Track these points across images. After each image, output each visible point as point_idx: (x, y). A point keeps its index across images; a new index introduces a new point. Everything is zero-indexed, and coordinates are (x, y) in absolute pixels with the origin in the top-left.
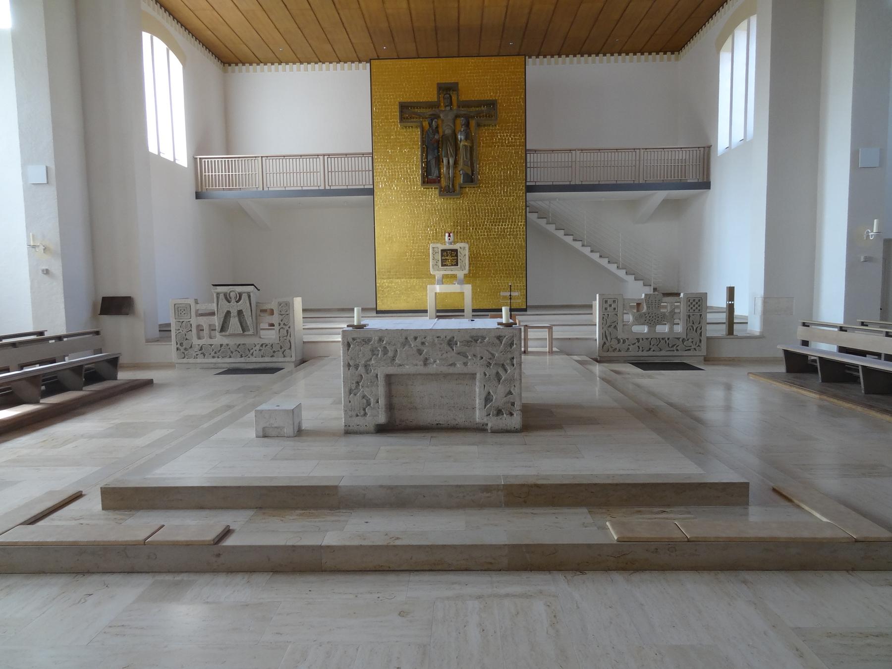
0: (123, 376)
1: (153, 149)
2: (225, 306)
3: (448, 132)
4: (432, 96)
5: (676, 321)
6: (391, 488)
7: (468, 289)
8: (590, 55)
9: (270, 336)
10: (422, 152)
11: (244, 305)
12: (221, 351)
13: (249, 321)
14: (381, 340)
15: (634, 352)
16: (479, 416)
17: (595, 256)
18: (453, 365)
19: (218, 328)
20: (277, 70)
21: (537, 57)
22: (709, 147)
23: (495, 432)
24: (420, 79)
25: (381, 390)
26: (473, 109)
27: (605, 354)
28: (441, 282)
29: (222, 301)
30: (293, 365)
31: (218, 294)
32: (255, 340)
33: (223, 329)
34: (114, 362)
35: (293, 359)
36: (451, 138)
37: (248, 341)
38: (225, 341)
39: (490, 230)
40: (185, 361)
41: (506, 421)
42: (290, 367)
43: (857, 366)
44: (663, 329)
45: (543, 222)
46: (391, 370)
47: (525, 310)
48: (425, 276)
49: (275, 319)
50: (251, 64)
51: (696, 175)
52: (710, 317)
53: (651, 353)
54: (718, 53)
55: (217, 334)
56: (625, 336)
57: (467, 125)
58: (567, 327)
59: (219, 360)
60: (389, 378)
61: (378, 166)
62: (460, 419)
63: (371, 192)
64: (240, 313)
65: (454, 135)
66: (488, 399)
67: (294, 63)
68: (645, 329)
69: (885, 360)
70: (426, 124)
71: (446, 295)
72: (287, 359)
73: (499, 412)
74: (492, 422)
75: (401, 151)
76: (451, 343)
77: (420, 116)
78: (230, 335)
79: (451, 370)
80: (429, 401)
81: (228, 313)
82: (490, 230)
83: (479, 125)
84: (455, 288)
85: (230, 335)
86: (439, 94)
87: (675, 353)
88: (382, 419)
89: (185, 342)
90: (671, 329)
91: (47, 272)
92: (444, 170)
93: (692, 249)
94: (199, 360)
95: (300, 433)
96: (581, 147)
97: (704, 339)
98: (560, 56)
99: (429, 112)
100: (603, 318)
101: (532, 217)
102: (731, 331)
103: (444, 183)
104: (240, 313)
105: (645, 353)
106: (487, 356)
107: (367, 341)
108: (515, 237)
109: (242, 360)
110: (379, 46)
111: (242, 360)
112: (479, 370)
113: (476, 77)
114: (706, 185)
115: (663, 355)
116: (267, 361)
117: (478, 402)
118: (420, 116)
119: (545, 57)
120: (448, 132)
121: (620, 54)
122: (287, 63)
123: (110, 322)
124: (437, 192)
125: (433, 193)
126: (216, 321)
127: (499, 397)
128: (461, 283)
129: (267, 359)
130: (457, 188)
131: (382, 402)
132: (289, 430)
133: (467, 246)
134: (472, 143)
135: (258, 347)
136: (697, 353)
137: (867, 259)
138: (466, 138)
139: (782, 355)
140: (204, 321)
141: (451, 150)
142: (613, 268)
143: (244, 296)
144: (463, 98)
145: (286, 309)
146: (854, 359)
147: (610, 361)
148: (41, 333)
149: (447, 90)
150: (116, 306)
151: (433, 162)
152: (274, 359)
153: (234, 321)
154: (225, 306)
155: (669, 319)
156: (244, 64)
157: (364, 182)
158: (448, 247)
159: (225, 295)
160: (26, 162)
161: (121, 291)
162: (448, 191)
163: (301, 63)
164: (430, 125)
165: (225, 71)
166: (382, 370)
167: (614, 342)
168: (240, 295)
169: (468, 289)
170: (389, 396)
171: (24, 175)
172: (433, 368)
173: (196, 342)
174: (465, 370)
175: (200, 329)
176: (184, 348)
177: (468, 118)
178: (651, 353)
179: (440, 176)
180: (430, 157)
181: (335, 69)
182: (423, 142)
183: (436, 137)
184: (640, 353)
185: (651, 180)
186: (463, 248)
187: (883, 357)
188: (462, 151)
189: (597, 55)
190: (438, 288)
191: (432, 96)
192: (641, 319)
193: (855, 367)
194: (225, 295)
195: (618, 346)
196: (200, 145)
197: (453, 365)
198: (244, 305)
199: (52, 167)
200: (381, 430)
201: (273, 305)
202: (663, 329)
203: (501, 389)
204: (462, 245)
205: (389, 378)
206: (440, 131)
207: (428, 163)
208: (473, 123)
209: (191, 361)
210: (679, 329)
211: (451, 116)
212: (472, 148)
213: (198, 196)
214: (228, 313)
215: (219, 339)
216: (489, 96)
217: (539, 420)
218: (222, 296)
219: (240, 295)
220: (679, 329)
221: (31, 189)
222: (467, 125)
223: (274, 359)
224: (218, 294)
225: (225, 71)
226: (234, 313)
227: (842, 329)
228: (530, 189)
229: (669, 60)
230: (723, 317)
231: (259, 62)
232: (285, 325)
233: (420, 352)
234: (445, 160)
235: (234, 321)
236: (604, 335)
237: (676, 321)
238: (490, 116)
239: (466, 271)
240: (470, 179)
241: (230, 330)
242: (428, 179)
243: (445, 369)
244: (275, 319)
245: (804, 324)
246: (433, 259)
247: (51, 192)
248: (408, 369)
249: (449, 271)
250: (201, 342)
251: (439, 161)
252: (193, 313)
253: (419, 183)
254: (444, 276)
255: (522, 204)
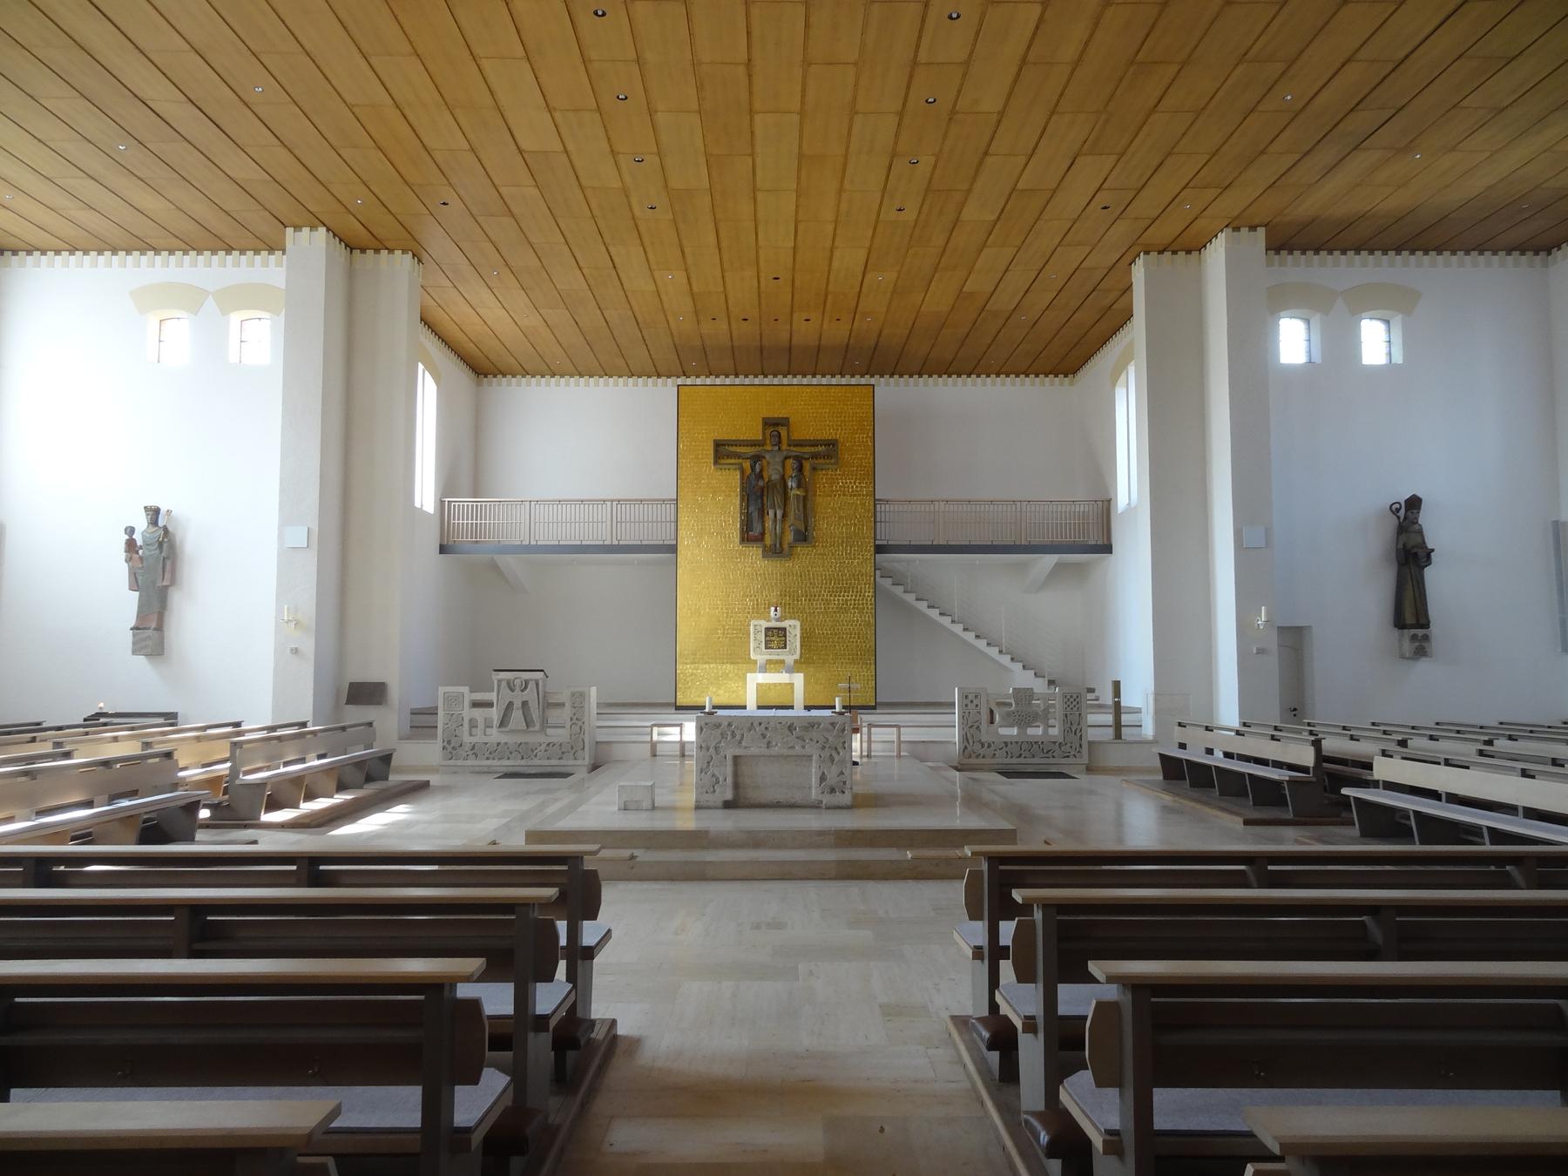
0: (394, 778)
1: (417, 504)
2: (507, 695)
3: (775, 477)
4: (756, 433)
5: (1051, 722)
6: (749, 832)
7: (798, 679)
8: (959, 375)
9: (560, 735)
10: (742, 500)
11: (530, 695)
12: (496, 751)
13: (535, 714)
14: (730, 725)
15: (1002, 759)
16: (814, 794)
17: (970, 637)
18: (792, 747)
19: (496, 722)
20: (548, 384)
21: (892, 375)
22: (1109, 501)
23: (828, 808)
24: (744, 403)
25: (729, 769)
26: (807, 449)
27: (967, 761)
28: (764, 669)
29: (505, 690)
30: (585, 770)
31: (499, 681)
32: (541, 739)
33: (503, 723)
34: (386, 759)
35: (587, 762)
36: (780, 487)
37: (532, 739)
38: (503, 739)
39: (828, 602)
40: (452, 762)
41: (840, 799)
42: (582, 773)
43: (1479, 827)
44: (1030, 731)
45: (899, 590)
46: (738, 752)
47: (874, 708)
48: (738, 657)
49: (566, 713)
50: (514, 376)
51: (1093, 538)
52: (1093, 718)
53: (1022, 760)
54: (1114, 385)
55: (494, 731)
56: (990, 740)
57: (800, 469)
58: (917, 728)
59: (495, 762)
60: (736, 759)
61: (684, 519)
62: (798, 797)
63: (673, 549)
64: (525, 704)
65: (783, 479)
66: (823, 778)
67: (572, 376)
68: (1015, 731)
69: (1526, 816)
70: (747, 465)
71: (769, 686)
72: (579, 762)
73: (833, 790)
74: (827, 799)
75: (713, 498)
76: (791, 728)
77: (738, 456)
78: (512, 731)
79: (791, 752)
80: (768, 779)
81: (511, 704)
82: (828, 602)
83: (814, 469)
84: (782, 678)
85: (512, 731)
86: (764, 430)
87: (1051, 761)
88: (729, 796)
89: (453, 740)
90: (1046, 732)
91: (295, 651)
92: (769, 524)
93: (1097, 628)
94: (469, 763)
95: (654, 808)
96: (945, 497)
97: (1085, 746)
98: (920, 376)
99: (750, 451)
100: (962, 717)
101: (886, 583)
102: (1118, 735)
103: (768, 540)
104: (525, 704)
105: (1015, 760)
106: (822, 740)
107: (718, 726)
108: (861, 611)
109: (523, 762)
110: (685, 360)
111: (523, 762)
112: (812, 750)
113: (807, 401)
114: (1108, 549)
115: (1038, 762)
116: (554, 764)
117: (814, 780)
118: (738, 456)
119: (901, 376)
120: (775, 477)
121: (998, 375)
122: (562, 376)
123: (357, 714)
124: (760, 551)
125: (755, 552)
126: (494, 714)
127: (832, 778)
128: (790, 670)
129: (554, 762)
130: (786, 546)
131: (730, 780)
132: (646, 804)
133: (798, 624)
134: (807, 491)
135: (543, 747)
136: (1078, 761)
137: (1261, 651)
138: (799, 486)
139: (1157, 763)
140: (478, 713)
141: (778, 500)
142: (993, 652)
143: (532, 685)
144: (796, 436)
145: (579, 699)
146: (1476, 816)
147: (973, 769)
148: (238, 725)
149: (774, 425)
150: (366, 693)
151: (755, 515)
152: (562, 762)
153: (517, 715)
154: (507, 695)
155: (1044, 717)
156: (504, 375)
157: (660, 536)
158: (773, 624)
159: (508, 683)
160: (285, 521)
161: (372, 676)
162: (775, 551)
163: (581, 376)
164: (753, 468)
165: (479, 384)
166: (730, 752)
167: (977, 747)
168: (527, 682)
169: (798, 679)
170: (736, 775)
171: (281, 537)
172: (775, 750)
173: (467, 739)
174: (803, 752)
175: (473, 724)
176: (452, 748)
177: (800, 460)
178: (1022, 760)
179: (763, 534)
180: (751, 509)
181: (626, 385)
182: (743, 489)
183: (761, 483)
184: (1008, 760)
185: (1036, 540)
186: (794, 627)
187: (1521, 812)
188: (793, 503)
189: (969, 375)
190: (762, 678)
191: (756, 433)
192: (1010, 720)
193: (1404, 813)
194: (508, 683)
195: (982, 752)
196: (447, 487)
197: (792, 747)
198: (527, 695)
199: (316, 529)
200: (727, 805)
201: (564, 697)
202: (1036, 732)
203: (835, 770)
204: (792, 622)
205: (736, 759)
206: (765, 475)
207: (748, 515)
208: (807, 466)
209: (460, 762)
210: (1054, 732)
211: (779, 459)
212: (805, 498)
213: (443, 549)
214: (511, 704)
215: (495, 735)
216: (826, 434)
217: (863, 802)
218: (504, 684)
219: (527, 682)
220: (1054, 732)
221: (287, 554)
222: (800, 469)
223: (562, 762)
224: (499, 681)
225: (479, 384)
226: (518, 704)
227: (1238, 733)
228: (879, 549)
229: (1062, 384)
230: (1109, 718)
231: (525, 373)
232: (577, 719)
233: (764, 736)
234: (771, 512)
235: (517, 715)
236: (965, 738)
237: (1051, 722)
238: (829, 457)
239: (797, 656)
240: (803, 537)
241: (511, 726)
242: (750, 534)
243: (785, 752)
244: (566, 713)
245: (1180, 725)
246: (756, 639)
247: (312, 558)
248: (754, 751)
249: (776, 654)
250: (474, 740)
251: (762, 513)
252: (467, 703)
253: (737, 540)
254: (769, 662)
255: (869, 568)
